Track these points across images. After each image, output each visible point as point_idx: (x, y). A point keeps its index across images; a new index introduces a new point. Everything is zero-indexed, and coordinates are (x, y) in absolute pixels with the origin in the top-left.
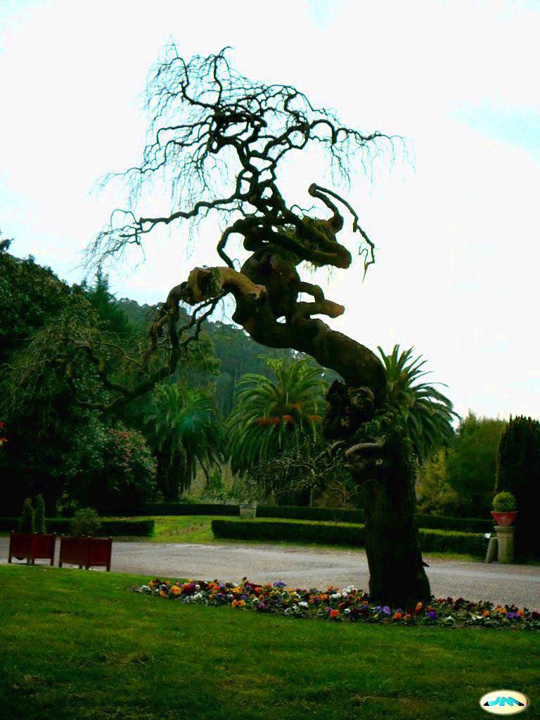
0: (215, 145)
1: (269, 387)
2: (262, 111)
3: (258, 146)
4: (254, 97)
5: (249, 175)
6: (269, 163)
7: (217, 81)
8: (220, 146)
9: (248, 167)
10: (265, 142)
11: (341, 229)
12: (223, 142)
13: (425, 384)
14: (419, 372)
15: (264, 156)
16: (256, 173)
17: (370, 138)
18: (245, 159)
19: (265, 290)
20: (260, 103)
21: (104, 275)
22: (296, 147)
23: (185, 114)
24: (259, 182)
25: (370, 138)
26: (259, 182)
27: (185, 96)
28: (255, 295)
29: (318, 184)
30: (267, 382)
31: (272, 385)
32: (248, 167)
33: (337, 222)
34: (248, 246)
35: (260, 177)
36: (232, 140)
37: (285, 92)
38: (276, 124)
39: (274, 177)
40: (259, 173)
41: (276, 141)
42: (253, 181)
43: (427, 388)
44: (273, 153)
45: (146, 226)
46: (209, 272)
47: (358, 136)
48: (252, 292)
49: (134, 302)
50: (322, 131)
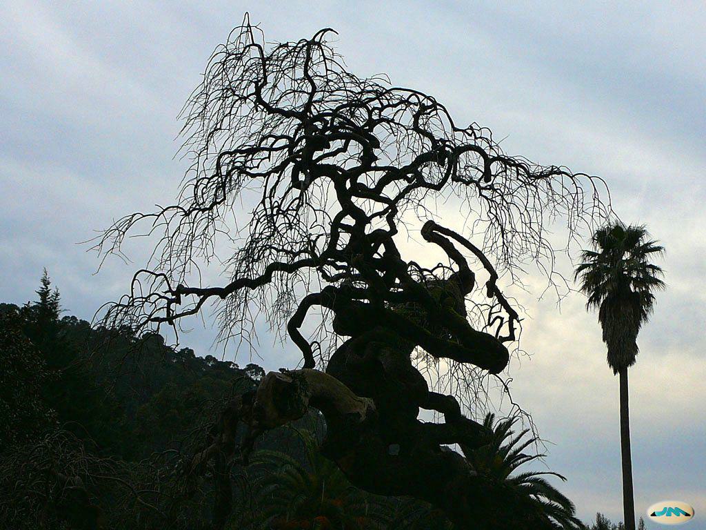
0: (302, 177)
1: (294, 471)
2: (371, 123)
3: (369, 179)
4: (363, 104)
5: (349, 221)
6: (380, 207)
7: (307, 77)
8: (311, 178)
9: (349, 209)
10: (380, 175)
11: (379, 230)
12: (317, 171)
13: (530, 474)
14: (523, 456)
15: (375, 194)
16: (362, 219)
17: (542, 176)
18: (344, 196)
19: (373, 406)
20: (370, 113)
21: (51, 293)
22: (430, 186)
23: (246, 123)
24: (382, 245)
25: (542, 176)
26: (382, 245)
27: (259, 101)
28: (358, 415)
29: (437, 221)
30: (291, 464)
31: (299, 470)
32: (349, 209)
33: (464, 280)
34: (339, 328)
35: (368, 226)
36: (331, 171)
37: (414, 99)
38: (395, 148)
39: (394, 230)
40: (368, 220)
41: (393, 174)
42: (356, 231)
43: (536, 481)
44: (390, 191)
45: (189, 301)
46: (290, 380)
47: (521, 171)
48: (354, 411)
49: (85, 324)
50: (471, 163)
